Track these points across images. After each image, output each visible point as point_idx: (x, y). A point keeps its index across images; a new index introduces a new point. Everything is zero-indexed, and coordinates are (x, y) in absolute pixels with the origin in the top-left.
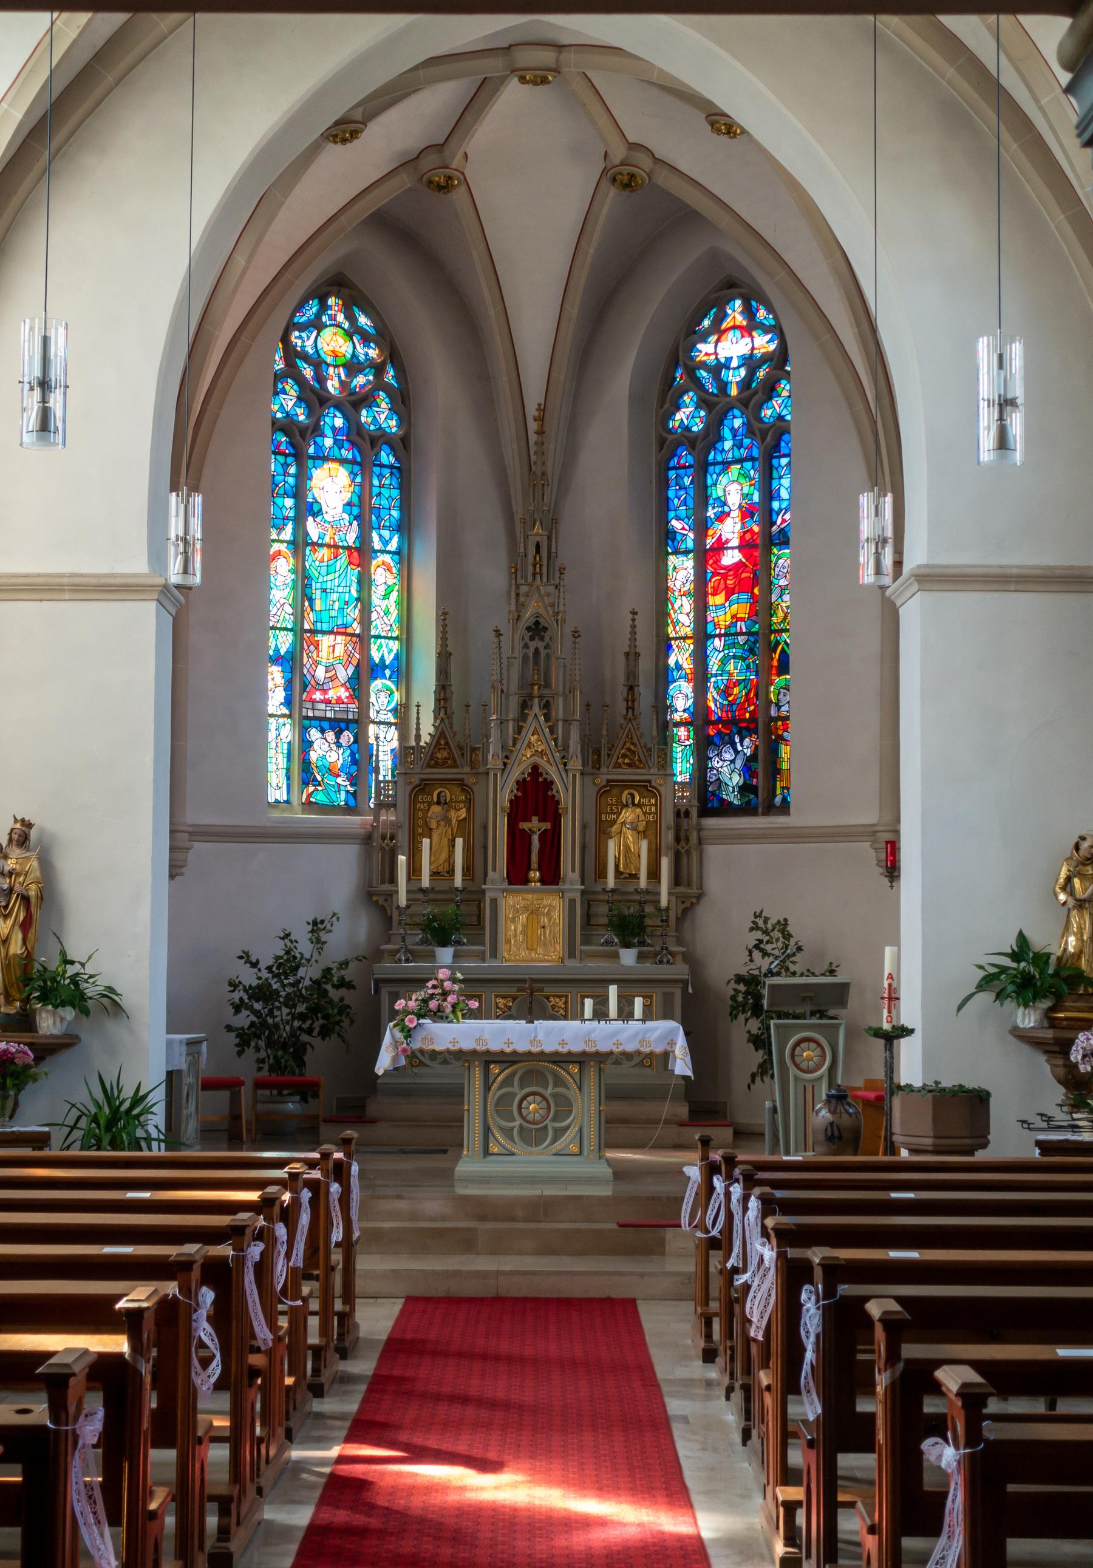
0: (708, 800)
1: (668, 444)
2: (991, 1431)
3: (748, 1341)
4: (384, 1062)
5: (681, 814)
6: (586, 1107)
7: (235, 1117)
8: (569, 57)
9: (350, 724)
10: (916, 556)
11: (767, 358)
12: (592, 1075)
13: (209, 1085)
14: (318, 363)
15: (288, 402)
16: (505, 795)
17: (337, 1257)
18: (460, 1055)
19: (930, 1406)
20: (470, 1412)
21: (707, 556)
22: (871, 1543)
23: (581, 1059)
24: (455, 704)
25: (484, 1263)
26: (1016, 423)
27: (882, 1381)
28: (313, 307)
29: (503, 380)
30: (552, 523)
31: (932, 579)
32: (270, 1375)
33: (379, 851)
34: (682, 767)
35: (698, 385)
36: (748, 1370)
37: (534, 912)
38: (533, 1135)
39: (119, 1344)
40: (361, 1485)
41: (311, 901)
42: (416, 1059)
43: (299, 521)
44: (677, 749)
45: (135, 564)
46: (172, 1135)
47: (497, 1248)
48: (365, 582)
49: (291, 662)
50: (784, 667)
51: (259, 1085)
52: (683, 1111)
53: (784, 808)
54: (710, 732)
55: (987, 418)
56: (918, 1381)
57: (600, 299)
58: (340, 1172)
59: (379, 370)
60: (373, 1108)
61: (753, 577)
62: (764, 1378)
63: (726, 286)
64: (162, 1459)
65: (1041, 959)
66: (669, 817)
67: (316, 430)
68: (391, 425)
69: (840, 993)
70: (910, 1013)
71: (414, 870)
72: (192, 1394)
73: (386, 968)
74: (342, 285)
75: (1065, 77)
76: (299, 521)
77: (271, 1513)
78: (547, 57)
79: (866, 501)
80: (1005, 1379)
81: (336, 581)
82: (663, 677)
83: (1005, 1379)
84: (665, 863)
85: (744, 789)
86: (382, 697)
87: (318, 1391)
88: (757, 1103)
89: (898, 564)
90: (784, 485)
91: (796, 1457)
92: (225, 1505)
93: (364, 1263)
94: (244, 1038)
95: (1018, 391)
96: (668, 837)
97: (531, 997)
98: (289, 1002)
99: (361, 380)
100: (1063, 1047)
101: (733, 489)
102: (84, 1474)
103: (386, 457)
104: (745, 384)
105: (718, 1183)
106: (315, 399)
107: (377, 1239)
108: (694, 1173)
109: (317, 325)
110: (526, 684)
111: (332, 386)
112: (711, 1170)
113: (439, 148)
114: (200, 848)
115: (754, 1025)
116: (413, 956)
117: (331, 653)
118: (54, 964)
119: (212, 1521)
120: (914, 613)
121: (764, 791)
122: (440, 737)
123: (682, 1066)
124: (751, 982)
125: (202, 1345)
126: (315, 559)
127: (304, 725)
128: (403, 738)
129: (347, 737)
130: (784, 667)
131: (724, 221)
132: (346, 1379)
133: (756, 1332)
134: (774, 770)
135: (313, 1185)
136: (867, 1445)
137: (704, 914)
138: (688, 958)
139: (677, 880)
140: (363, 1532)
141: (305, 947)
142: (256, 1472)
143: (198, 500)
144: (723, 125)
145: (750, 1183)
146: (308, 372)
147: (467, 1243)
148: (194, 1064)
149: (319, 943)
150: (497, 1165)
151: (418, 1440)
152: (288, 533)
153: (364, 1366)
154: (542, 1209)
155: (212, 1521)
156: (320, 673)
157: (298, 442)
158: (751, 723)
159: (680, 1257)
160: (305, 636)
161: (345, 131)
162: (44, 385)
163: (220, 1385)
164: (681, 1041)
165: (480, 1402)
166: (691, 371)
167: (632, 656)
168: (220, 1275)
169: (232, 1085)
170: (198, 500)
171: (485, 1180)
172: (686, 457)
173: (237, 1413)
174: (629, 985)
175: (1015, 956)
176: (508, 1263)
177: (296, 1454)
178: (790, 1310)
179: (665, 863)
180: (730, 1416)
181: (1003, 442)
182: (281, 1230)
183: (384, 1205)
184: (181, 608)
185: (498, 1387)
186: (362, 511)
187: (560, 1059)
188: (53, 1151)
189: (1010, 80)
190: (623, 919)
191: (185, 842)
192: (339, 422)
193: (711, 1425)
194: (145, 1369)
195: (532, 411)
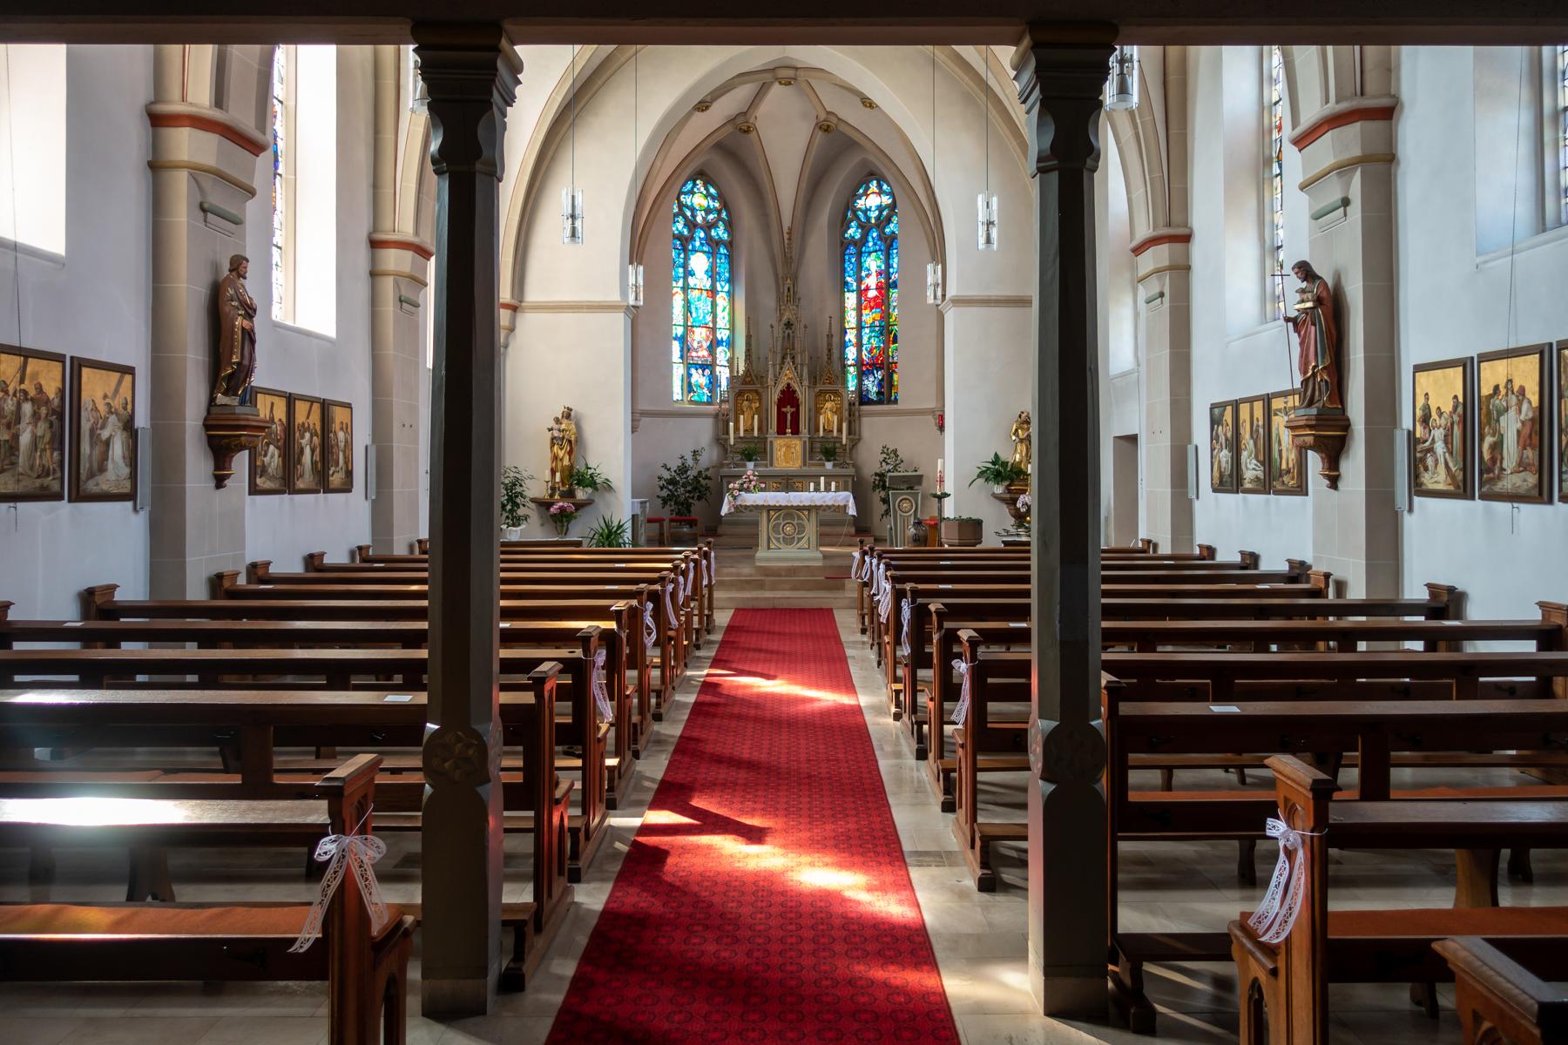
0: (863, 398)
1: (845, 244)
2: (981, 657)
3: (880, 623)
4: (725, 510)
5: (851, 404)
6: (811, 529)
7: (662, 534)
8: (801, 73)
9: (708, 366)
10: (952, 291)
11: (887, 206)
12: (813, 515)
13: (650, 521)
14: (693, 209)
15: (680, 226)
16: (776, 397)
17: (705, 591)
18: (757, 507)
19: (956, 649)
20: (762, 655)
21: (861, 293)
22: (931, 705)
23: (809, 508)
24: (754, 357)
25: (768, 594)
26: (994, 233)
27: (935, 637)
28: (689, 185)
29: (773, 216)
30: (795, 279)
31: (959, 302)
32: (677, 639)
33: (721, 422)
34: (852, 384)
35: (858, 218)
36: (880, 637)
37: (788, 447)
38: (789, 540)
39: (612, 625)
40: (716, 686)
41: (693, 443)
42: (739, 509)
43: (685, 278)
44: (850, 377)
45: (615, 297)
46: (635, 541)
47: (774, 588)
48: (714, 305)
49: (683, 340)
50: (895, 341)
51: (672, 520)
52: (853, 530)
53: (896, 402)
54: (864, 370)
55: (982, 231)
56: (951, 638)
57: (815, 181)
58: (706, 555)
59: (719, 212)
60: (720, 530)
61: (882, 302)
62: (886, 639)
63: (870, 174)
64: (631, 674)
65: (1005, 464)
66: (846, 406)
67: (693, 239)
68: (725, 236)
69: (919, 479)
70: (949, 487)
71: (737, 429)
72: (644, 647)
73: (725, 471)
74: (702, 174)
75: (1013, 73)
76: (685, 278)
77: (678, 697)
78: (791, 73)
79: (930, 267)
80: (988, 637)
81: (702, 306)
82: (843, 345)
83: (988, 637)
84: (845, 425)
85: (879, 393)
86: (722, 355)
87: (698, 647)
88: (884, 526)
89: (944, 296)
90: (895, 262)
91: (900, 672)
92: (659, 694)
93: (716, 595)
94: (665, 501)
95: (995, 218)
96: (846, 414)
97: (787, 482)
98: (684, 485)
99: (711, 217)
100: (1014, 501)
101: (873, 263)
102: (598, 679)
103: (723, 250)
104: (878, 218)
105: (867, 559)
106: (692, 225)
107: (721, 583)
108: (857, 554)
109: (692, 192)
110: (784, 349)
111: (699, 219)
112: (864, 553)
113: (745, 114)
114: (645, 420)
115: (883, 494)
116: (737, 466)
117: (700, 336)
118: (583, 469)
119: (653, 701)
120: (950, 316)
121: (887, 394)
122: (747, 372)
123: (852, 511)
124: (881, 475)
125: (648, 627)
126: (693, 295)
127: (688, 367)
128: (731, 372)
129: (707, 372)
130: (895, 341)
131: (868, 146)
132: (712, 642)
133: (883, 620)
134: (891, 385)
135: (695, 561)
136: (929, 666)
137: (861, 446)
138: (854, 465)
139: (850, 432)
140: (717, 705)
141: (690, 462)
142: (672, 681)
143: (641, 268)
144: (868, 103)
145: (880, 558)
146: (688, 213)
147: (760, 585)
148: (643, 511)
149: (696, 460)
150: (773, 553)
151: (740, 667)
152: (681, 283)
153: (717, 637)
154: (792, 571)
155: (653, 701)
156: (695, 345)
157: (685, 242)
158: (882, 365)
159: (851, 591)
160: (688, 328)
161: (703, 106)
162: (573, 217)
163: (656, 644)
164: (851, 500)
165: (767, 651)
166: (854, 212)
167: (830, 336)
168: (655, 597)
169: (660, 521)
170: (641, 268)
171: (768, 560)
172: (852, 250)
173: (663, 657)
174: (829, 477)
175: (993, 463)
176: (779, 594)
177: (689, 673)
178: (897, 609)
179: (845, 425)
180: (872, 656)
181: (988, 241)
182: (681, 579)
183: (725, 570)
184: (635, 315)
185: (775, 645)
186: (713, 274)
187: (799, 508)
188: (584, 548)
189: (992, 82)
190: (826, 450)
191: (638, 417)
192: (702, 235)
193: (864, 660)
194: (624, 636)
195: (786, 230)
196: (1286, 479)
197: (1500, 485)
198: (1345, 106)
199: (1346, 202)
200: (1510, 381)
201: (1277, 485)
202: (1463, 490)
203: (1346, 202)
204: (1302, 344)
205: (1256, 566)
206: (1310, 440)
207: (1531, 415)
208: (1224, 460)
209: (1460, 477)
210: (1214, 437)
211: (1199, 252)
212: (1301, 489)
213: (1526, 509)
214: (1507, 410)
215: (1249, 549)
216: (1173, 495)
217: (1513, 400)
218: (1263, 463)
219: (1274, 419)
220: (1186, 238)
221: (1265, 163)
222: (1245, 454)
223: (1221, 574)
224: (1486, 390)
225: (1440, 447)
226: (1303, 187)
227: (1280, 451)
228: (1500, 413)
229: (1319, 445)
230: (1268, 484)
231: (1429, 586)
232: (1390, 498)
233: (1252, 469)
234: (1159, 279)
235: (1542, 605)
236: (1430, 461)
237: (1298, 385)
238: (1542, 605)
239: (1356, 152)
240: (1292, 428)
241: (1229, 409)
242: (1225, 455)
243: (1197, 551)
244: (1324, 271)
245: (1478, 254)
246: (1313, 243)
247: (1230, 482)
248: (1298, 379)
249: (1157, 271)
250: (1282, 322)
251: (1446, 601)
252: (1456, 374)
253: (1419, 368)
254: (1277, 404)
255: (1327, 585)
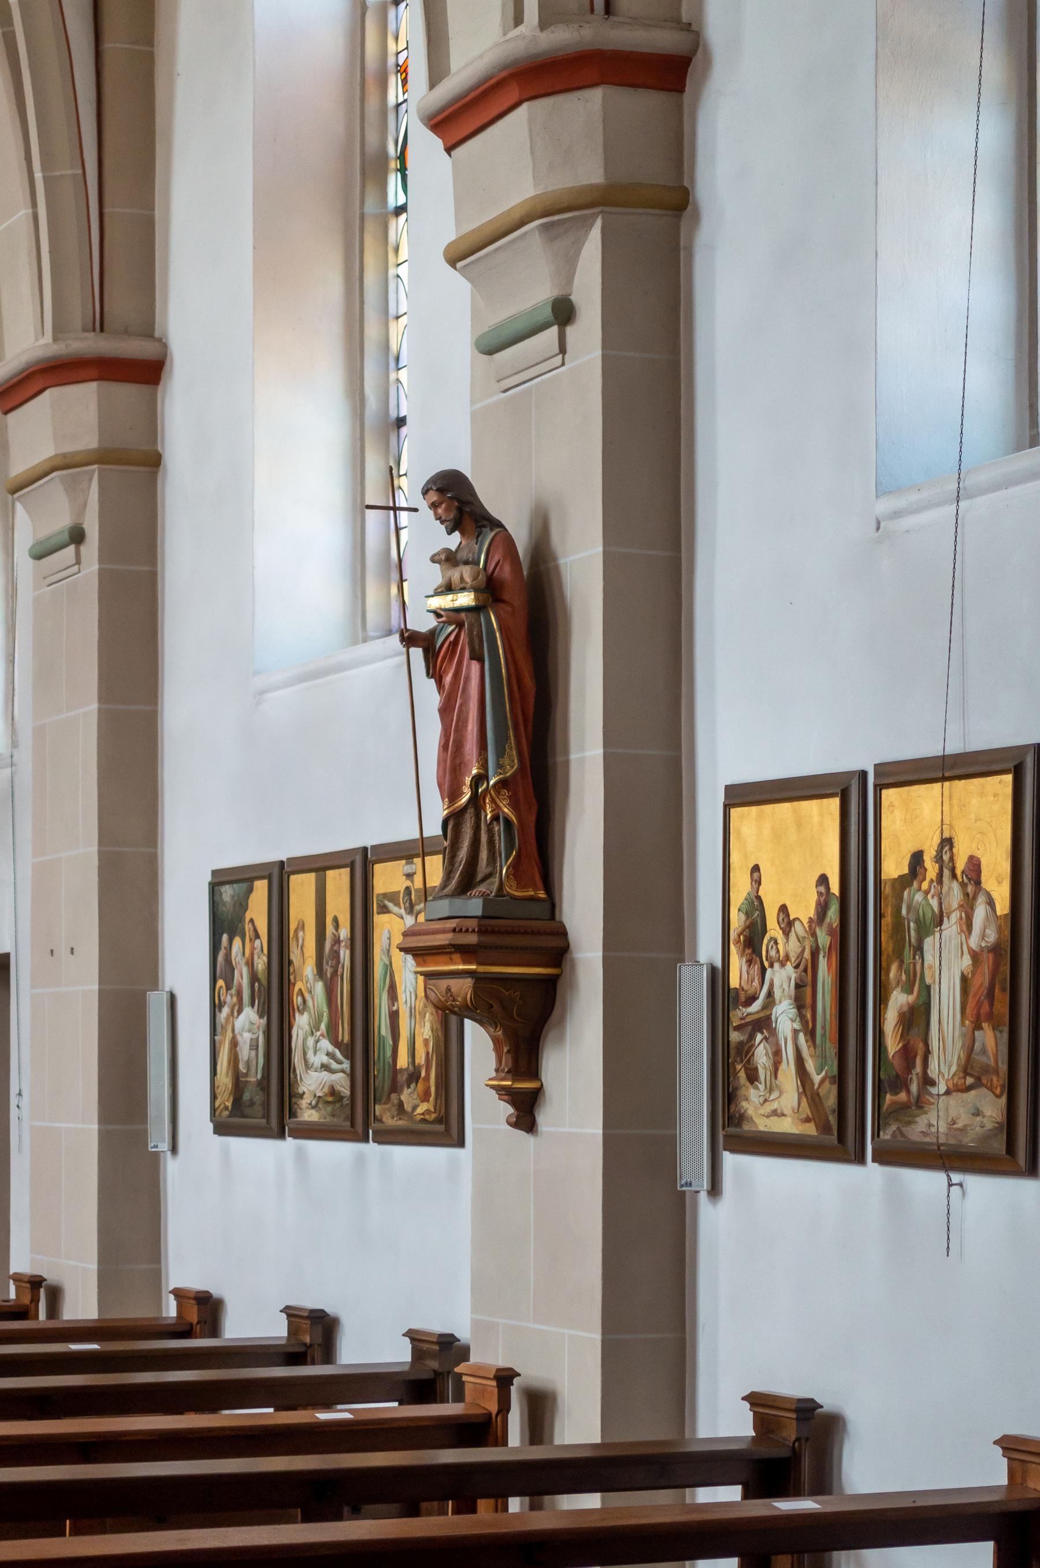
196: (408, 1097)
197: (921, 1123)
198: (562, 37)
199: (563, 313)
200: (947, 842)
201: (386, 1115)
202: (836, 1137)
203: (563, 313)
204: (445, 711)
205: (328, 1354)
206: (463, 988)
207: (992, 937)
208: (245, 1039)
209: (831, 1101)
210: (220, 971)
211: (184, 409)
212: (446, 1128)
213: (982, 1190)
214: (939, 920)
215: (310, 1302)
216: (105, 1138)
217: (954, 894)
218: (349, 1051)
219: (380, 921)
220: (149, 372)
221: (370, 166)
222: (302, 1022)
223: (234, 1375)
224: (894, 867)
225: (785, 1017)
226: (458, 256)
227: (394, 1016)
228: (924, 931)
229: (492, 1002)
230: (362, 1113)
231: (755, 1400)
232: (664, 1155)
233: (319, 1071)
234: (72, 488)
235: (1010, 1445)
236: (761, 1056)
237: (433, 828)
238: (1010, 1445)
239: (591, 172)
240: (420, 953)
241: (261, 887)
242: (248, 1024)
243: (171, 1309)
244: (504, 503)
245: (881, 492)
246: (480, 421)
247: (260, 1105)
248: (436, 810)
249: (64, 463)
250: (396, 637)
251: (795, 1442)
252: (823, 815)
253: (741, 796)
254: (388, 878)
255: (504, 1407)
